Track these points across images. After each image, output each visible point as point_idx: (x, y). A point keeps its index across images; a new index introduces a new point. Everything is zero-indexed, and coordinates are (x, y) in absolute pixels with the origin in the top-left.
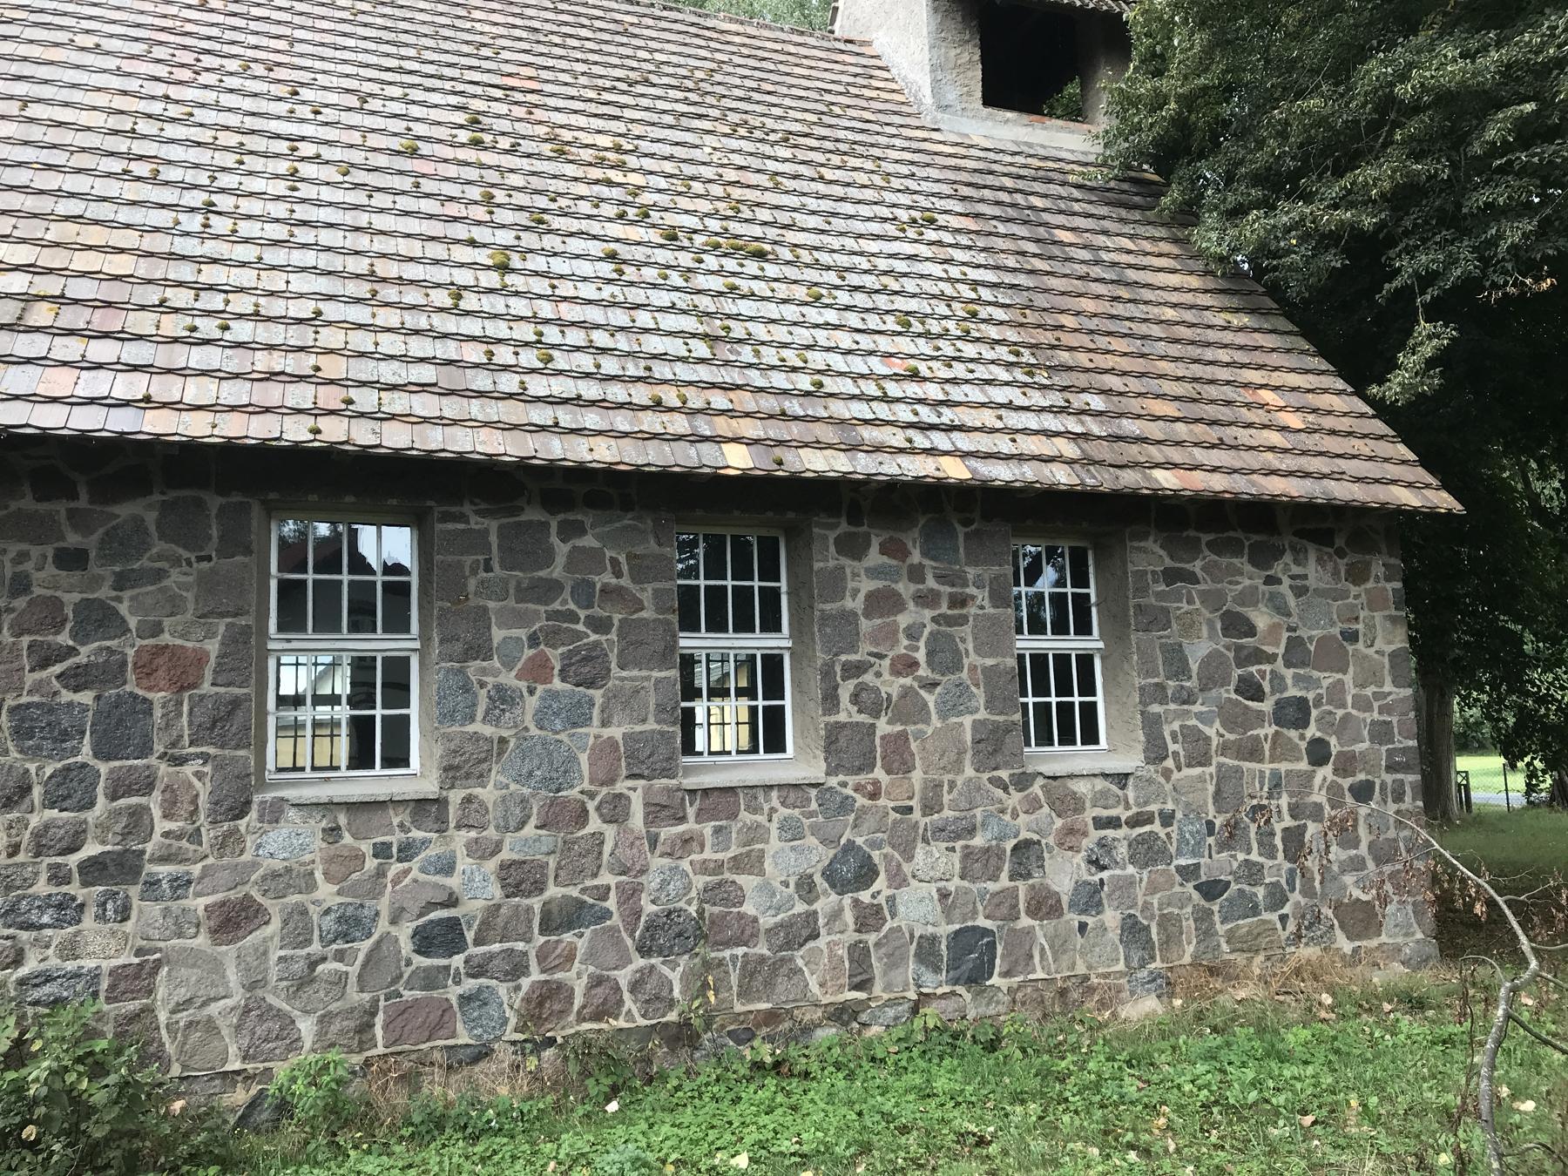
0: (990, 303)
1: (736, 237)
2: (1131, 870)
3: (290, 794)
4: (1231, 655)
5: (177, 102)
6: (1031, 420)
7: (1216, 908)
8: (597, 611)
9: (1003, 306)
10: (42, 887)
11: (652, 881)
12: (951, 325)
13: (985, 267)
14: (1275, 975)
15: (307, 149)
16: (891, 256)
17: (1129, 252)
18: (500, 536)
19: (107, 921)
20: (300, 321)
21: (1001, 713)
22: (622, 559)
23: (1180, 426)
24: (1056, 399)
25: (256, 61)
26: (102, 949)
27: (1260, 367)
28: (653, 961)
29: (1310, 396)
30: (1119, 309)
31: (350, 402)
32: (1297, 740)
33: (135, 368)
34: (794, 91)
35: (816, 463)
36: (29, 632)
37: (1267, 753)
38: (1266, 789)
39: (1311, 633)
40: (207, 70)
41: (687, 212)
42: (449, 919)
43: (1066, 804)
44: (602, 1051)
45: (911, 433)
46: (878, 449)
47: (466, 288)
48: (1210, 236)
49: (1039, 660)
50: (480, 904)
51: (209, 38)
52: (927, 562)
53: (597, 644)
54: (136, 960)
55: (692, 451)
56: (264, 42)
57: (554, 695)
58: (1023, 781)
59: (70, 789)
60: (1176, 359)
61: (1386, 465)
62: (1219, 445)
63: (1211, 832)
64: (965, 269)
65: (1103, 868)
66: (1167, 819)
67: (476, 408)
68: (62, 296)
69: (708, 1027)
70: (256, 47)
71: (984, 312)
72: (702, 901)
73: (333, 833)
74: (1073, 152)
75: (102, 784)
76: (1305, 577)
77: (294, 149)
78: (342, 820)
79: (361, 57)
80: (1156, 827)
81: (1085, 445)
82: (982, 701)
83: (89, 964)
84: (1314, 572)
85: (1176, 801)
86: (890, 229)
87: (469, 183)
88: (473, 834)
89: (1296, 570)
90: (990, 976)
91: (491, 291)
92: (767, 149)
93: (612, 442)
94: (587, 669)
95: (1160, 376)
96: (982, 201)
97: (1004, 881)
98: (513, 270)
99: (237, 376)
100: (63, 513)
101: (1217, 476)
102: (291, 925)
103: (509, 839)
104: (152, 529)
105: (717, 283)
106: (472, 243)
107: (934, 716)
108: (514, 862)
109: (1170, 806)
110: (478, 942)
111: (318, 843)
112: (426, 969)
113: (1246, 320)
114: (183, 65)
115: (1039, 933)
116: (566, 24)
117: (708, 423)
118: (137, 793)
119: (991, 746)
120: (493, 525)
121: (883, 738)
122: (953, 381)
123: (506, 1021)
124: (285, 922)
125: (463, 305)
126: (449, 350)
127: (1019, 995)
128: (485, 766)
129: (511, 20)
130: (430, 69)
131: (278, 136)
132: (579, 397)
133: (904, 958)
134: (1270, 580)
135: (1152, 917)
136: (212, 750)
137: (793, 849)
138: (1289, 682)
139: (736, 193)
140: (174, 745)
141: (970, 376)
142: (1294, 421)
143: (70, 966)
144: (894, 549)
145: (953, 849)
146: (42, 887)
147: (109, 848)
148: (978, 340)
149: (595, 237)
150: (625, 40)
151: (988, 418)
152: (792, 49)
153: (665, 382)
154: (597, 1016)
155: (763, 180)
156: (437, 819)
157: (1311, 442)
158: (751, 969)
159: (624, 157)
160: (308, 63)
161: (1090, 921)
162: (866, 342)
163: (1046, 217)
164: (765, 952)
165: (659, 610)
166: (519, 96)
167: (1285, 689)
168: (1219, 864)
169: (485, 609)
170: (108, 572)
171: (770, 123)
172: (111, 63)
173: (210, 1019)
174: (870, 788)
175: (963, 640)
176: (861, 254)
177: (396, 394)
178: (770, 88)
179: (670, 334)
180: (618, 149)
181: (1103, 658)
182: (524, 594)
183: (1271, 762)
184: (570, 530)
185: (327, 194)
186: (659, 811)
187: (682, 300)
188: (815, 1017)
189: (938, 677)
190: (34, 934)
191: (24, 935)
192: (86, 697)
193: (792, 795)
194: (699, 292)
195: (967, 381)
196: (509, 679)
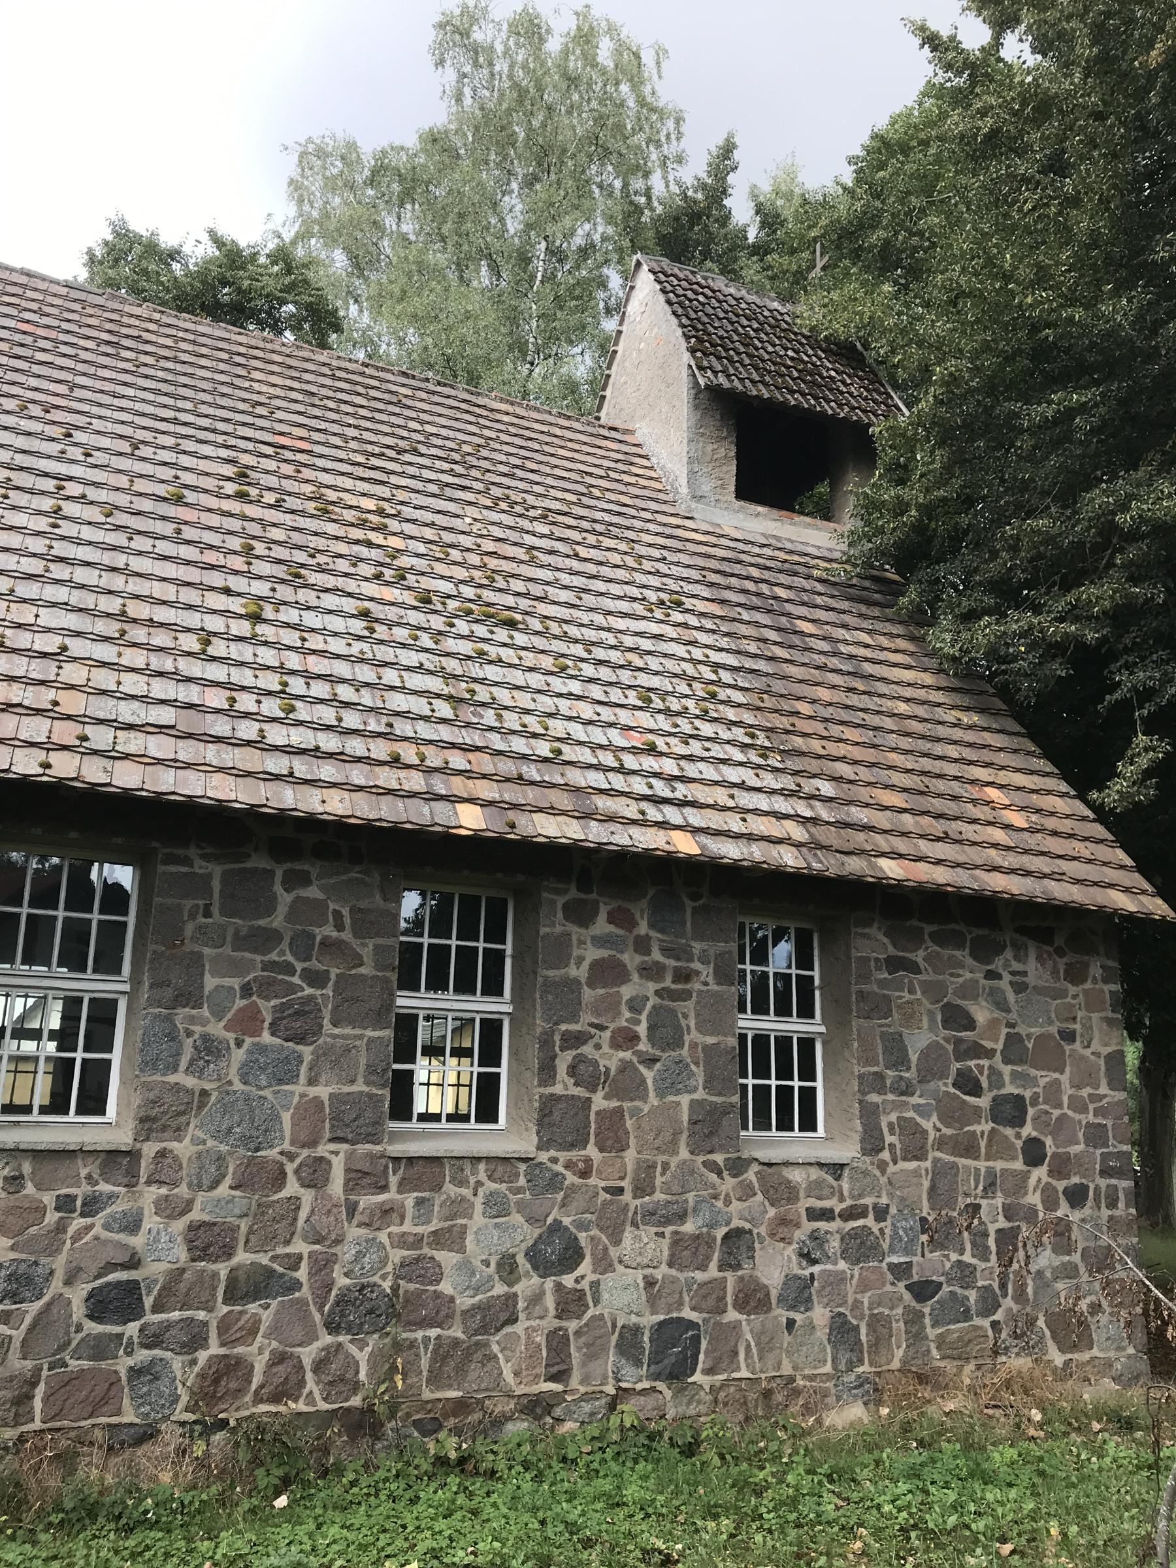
1: (489, 605)
2: (842, 1265)
4: (950, 1048)
6: (763, 802)
7: (927, 1310)
8: (315, 964)
9: (742, 689)
11: (346, 1252)
12: (690, 704)
13: (727, 651)
15: (73, 489)
16: (638, 634)
17: (867, 646)
20: (44, 655)
21: (720, 1094)
22: (345, 912)
23: (907, 817)
24: (788, 782)
25: (34, 402)
27: (988, 765)
28: (341, 1339)
30: (853, 700)
31: (85, 738)
34: (557, 472)
35: (548, 828)
39: (1030, 1031)
43: (778, 1190)
45: (644, 805)
46: (611, 818)
47: (215, 634)
48: (943, 638)
49: (761, 1041)
50: (163, 1266)
52: (653, 934)
53: (311, 998)
55: (426, 810)
57: (262, 1049)
58: (737, 1166)
60: (907, 752)
65: (814, 1262)
66: (881, 1213)
67: (212, 754)
69: (392, 1415)
71: (723, 694)
72: (397, 1277)
76: (1025, 973)
78: (27, 1168)
80: (869, 1221)
81: (813, 830)
84: (1034, 970)
85: (891, 1195)
86: (639, 608)
87: (231, 533)
88: (164, 1191)
89: (1016, 966)
91: (241, 639)
92: (525, 524)
93: (346, 795)
94: (298, 1024)
95: (890, 768)
97: (713, 1272)
98: (265, 621)
101: (941, 869)
103: (201, 1197)
105: (466, 648)
106: (227, 591)
107: (652, 1094)
108: (203, 1224)
109: (884, 1200)
110: (156, 1309)
112: (99, 1337)
113: (975, 718)
115: (745, 1328)
116: (342, 390)
117: (445, 782)
119: (708, 1127)
120: (216, 871)
121: (598, 1113)
122: (689, 758)
123: (176, 1399)
125: (211, 650)
126: (192, 694)
127: (722, 1394)
128: (183, 1119)
129: (289, 383)
130: (205, 422)
131: (46, 475)
132: (317, 749)
133: (605, 1349)
135: (862, 1318)
137: (496, 1226)
138: (1007, 1078)
139: (493, 563)
142: (1018, 820)
144: (621, 918)
145: (662, 1235)
148: (715, 720)
149: (350, 595)
150: (397, 410)
151: (720, 796)
152: (558, 432)
153: (406, 739)
154: (275, 1398)
155: (520, 553)
156: (128, 1172)
157: (1032, 841)
158: (444, 1352)
160: (86, 408)
161: (798, 1317)
162: (607, 714)
163: (789, 607)
164: (460, 1334)
165: (376, 968)
166: (288, 455)
167: (1003, 1085)
168: (932, 1263)
169: (200, 956)
171: (531, 500)
175: (686, 1016)
176: (609, 630)
177: (133, 734)
178: (534, 466)
180: (381, 512)
181: (824, 1044)
183: (988, 1159)
184: (294, 880)
185: (87, 533)
186: (362, 1178)
187: (429, 661)
189: (658, 1053)
194: (448, 654)
195: (702, 759)
196: (217, 1029)
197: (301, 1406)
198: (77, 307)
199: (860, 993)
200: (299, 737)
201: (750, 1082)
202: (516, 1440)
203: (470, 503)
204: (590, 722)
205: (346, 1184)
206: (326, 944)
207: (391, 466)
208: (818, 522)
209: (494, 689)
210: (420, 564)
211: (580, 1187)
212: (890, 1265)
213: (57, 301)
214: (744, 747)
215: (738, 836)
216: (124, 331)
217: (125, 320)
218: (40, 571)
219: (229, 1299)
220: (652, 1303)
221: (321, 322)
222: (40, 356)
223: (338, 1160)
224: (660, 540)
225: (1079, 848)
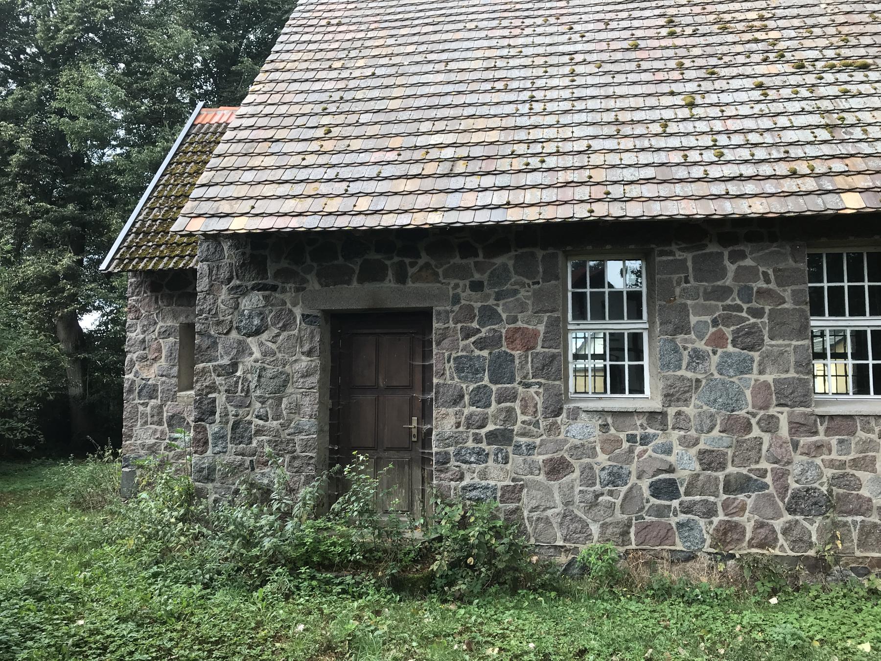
1: (846, 58)
5: (514, 47)
8: (754, 304)
10: (470, 444)
11: (795, 469)
15: (579, 58)
19: (499, 463)
20: (580, 152)
22: (770, 272)
25: (551, 16)
26: (498, 477)
28: (797, 517)
31: (608, 193)
36: (461, 322)
41: (810, 49)
47: (669, 120)
50: (687, 472)
51: (528, 10)
53: (754, 325)
54: (513, 484)
57: (729, 355)
59: (480, 398)
67: (679, 189)
69: (837, 563)
70: (551, 8)
72: (830, 485)
73: (605, 427)
75: (493, 396)
77: (572, 59)
78: (610, 420)
83: (492, 483)
88: (682, 433)
91: (685, 120)
93: (764, 200)
94: (749, 340)
98: (697, 105)
99: (550, 186)
102: (585, 474)
103: (703, 437)
104: (512, 269)
108: (706, 451)
110: (687, 494)
111: (597, 432)
114: (516, 27)
120: (689, 257)
123: (704, 541)
124: (582, 472)
126: (662, 157)
128: (688, 395)
131: (564, 54)
132: (741, 175)
136: (543, 381)
139: (845, 30)
140: (525, 377)
143: (484, 483)
146: (470, 444)
147: (498, 427)
149: (748, 76)
153: (799, 159)
154: (761, 546)
155: (865, 18)
159: (766, 23)
164: (877, 520)
169: (686, 305)
172: (483, 34)
173: (547, 518)
177: (633, 186)
179: (801, 128)
180: (761, 18)
182: (708, 296)
185: (590, 80)
186: (796, 427)
187: (808, 106)
191: (464, 466)
192: (485, 353)
194: (821, 98)
196: (701, 345)
200: (729, 170)
206: (760, 292)
210: (793, 44)
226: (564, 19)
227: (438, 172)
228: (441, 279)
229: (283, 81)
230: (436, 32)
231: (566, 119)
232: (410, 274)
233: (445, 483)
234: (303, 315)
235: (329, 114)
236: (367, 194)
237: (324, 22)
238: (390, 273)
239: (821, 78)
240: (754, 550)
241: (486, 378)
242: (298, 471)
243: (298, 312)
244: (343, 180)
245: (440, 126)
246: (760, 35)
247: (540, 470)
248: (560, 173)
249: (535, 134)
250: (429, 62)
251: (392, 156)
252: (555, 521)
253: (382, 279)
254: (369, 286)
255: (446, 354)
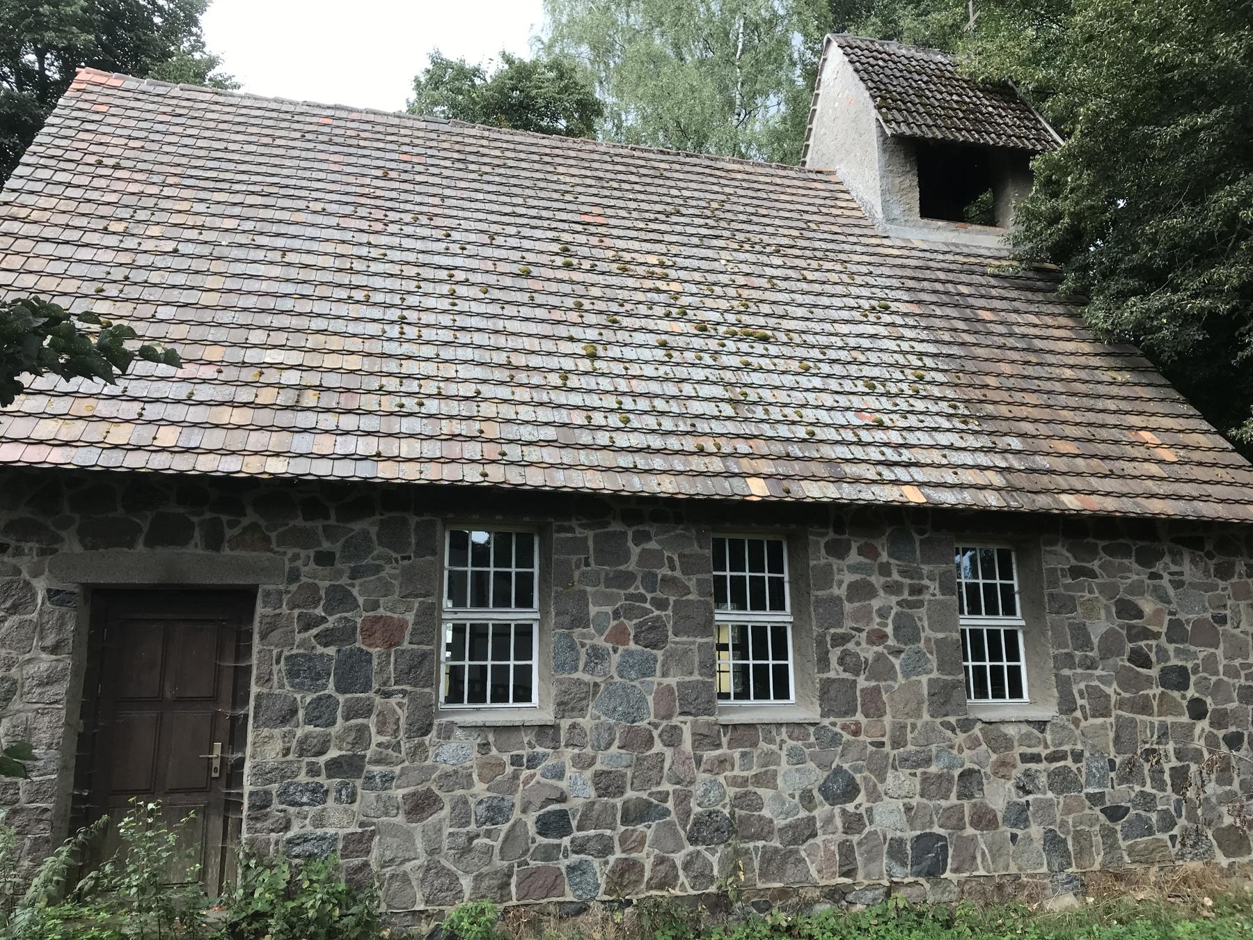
0: (933, 369)
1: (747, 326)
2: (1050, 795)
3: (458, 719)
4: (1124, 632)
5: (376, 246)
6: (968, 459)
7: (1118, 828)
8: (658, 594)
9: (942, 371)
10: (303, 778)
11: (698, 790)
12: (904, 386)
13: (928, 341)
14: (1167, 882)
15: (460, 275)
16: (858, 336)
17: (1035, 326)
18: (595, 542)
19: (342, 803)
20: (467, 398)
21: (950, 674)
22: (676, 557)
23: (1079, 461)
24: (985, 441)
25: (421, 213)
26: (339, 822)
27: (1140, 413)
28: (699, 848)
29: (1181, 435)
30: (1029, 371)
31: (504, 454)
32: (1179, 699)
33: (369, 433)
34: (782, 214)
35: (813, 491)
36: (299, 607)
37: (1156, 709)
38: (1155, 736)
39: (1188, 617)
40: (392, 222)
41: (712, 309)
42: (560, 811)
43: (999, 743)
44: (667, 912)
45: (880, 468)
46: (857, 480)
47: (570, 371)
48: (1096, 314)
49: (976, 634)
50: (581, 801)
51: (391, 199)
52: (892, 561)
53: (659, 617)
54: (360, 830)
55: (727, 484)
56: (426, 199)
57: (630, 653)
58: (966, 725)
59: (321, 713)
60: (1075, 409)
61: (1244, 489)
62: (1110, 475)
63: (1112, 768)
64: (913, 343)
65: (1029, 793)
66: (1078, 757)
67: (583, 457)
68: (321, 386)
69: (738, 898)
70: (421, 204)
71: (929, 376)
72: (733, 806)
73: (484, 747)
74: (989, 249)
75: (340, 710)
76: (1181, 574)
77: (451, 276)
78: (491, 738)
79: (488, 207)
80: (1069, 762)
81: (1008, 476)
82: (935, 665)
83: (331, 831)
84: (1189, 570)
85: (1084, 743)
86: (857, 315)
87: (566, 295)
88: (576, 751)
89: (1174, 568)
90: (944, 872)
91: (586, 373)
92: (764, 259)
93: (673, 478)
94: (652, 636)
95: (1063, 422)
96: (922, 290)
97: (953, 800)
98: (599, 358)
99: (431, 437)
100: (321, 528)
101: (1109, 499)
102: (457, 811)
103: (600, 755)
104: (374, 538)
105: (735, 361)
106: (571, 339)
107: (900, 676)
108: (603, 772)
109: (1079, 747)
110: (580, 828)
111: (475, 754)
112: (545, 846)
113: (1127, 376)
114: (377, 220)
115: (980, 840)
116: (621, 172)
117: (737, 463)
118: (361, 716)
119: (942, 698)
120: (590, 534)
121: (862, 690)
122: (909, 429)
123: (598, 886)
124: (453, 809)
125: (569, 384)
126: (562, 416)
127: (967, 887)
128: (584, 702)
129: (583, 172)
130: (533, 212)
131: (440, 267)
132: (649, 447)
133: (880, 854)
134: (1154, 576)
135: (1068, 833)
136: (408, 688)
137: (797, 770)
138: (1171, 654)
139: (745, 293)
140: (385, 684)
141: (921, 425)
142: (1169, 455)
143: (319, 832)
144: (869, 551)
145: (915, 775)
146: (303, 778)
147: (344, 753)
148: (925, 397)
149: (651, 331)
150: (661, 182)
151: (936, 456)
152: (778, 181)
153: (705, 434)
154: (661, 887)
155: (763, 282)
156: (553, 740)
157: (1182, 471)
158: (769, 857)
159: (666, 271)
160: (454, 213)
161: (1019, 832)
162: (843, 401)
163: (971, 301)
164: (778, 845)
165: (700, 594)
166: (593, 229)
167: (1168, 659)
168: (1120, 793)
169: (585, 592)
170: (346, 567)
171: (766, 239)
172: (333, 221)
173: (405, 873)
174: (853, 727)
175: (920, 619)
176: (836, 335)
177: (532, 448)
178: (764, 212)
179: (706, 399)
180: (662, 265)
181: (1024, 633)
182: (609, 582)
183: (1159, 715)
184: (641, 538)
185: (476, 308)
186: (704, 739)
187: (713, 375)
188: (815, 895)
189: (903, 646)
190: (298, 809)
191: (292, 810)
192: (331, 651)
193: (797, 731)
194: (724, 368)
195: (919, 429)
196: (600, 641)
197: (677, 892)
198: (434, 136)
199: (1051, 595)
200: (636, 440)
201: (970, 664)
202: (824, 916)
203: (723, 248)
204: (832, 409)
205: (693, 744)
206: (665, 580)
207: (664, 227)
208: (987, 228)
209: (759, 390)
210: (695, 301)
211: (853, 742)
212: (1087, 795)
213: (421, 134)
214: (949, 416)
215: (953, 486)
216: (468, 149)
217: (467, 140)
218: (451, 339)
219: (625, 821)
220: (911, 822)
221: (588, 110)
222: (419, 178)
223: (687, 727)
224: (866, 259)
225: (1221, 474)
226: (438, 221)
227: (278, 402)
228: (274, 546)
229: (27, 237)
230: (266, 207)
231: (447, 353)
232: (227, 537)
233: (262, 836)
234: (49, 591)
235: (107, 298)
236: (173, 423)
237: (92, 159)
238: (197, 534)
239: (723, 345)
240: (654, 893)
241: (331, 685)
242: (21, 833)
243: (41, 586)
244: (135, 399)
245: (279, 338)
246: (661, 285)
247: (398, 809)
248: (443, 422)
249: (410, 367)
250: (259, 247)
251: (209, 372)
252: (414, 879)
253: (184, 542)
254: (163, 552)
255: (275, 653)
